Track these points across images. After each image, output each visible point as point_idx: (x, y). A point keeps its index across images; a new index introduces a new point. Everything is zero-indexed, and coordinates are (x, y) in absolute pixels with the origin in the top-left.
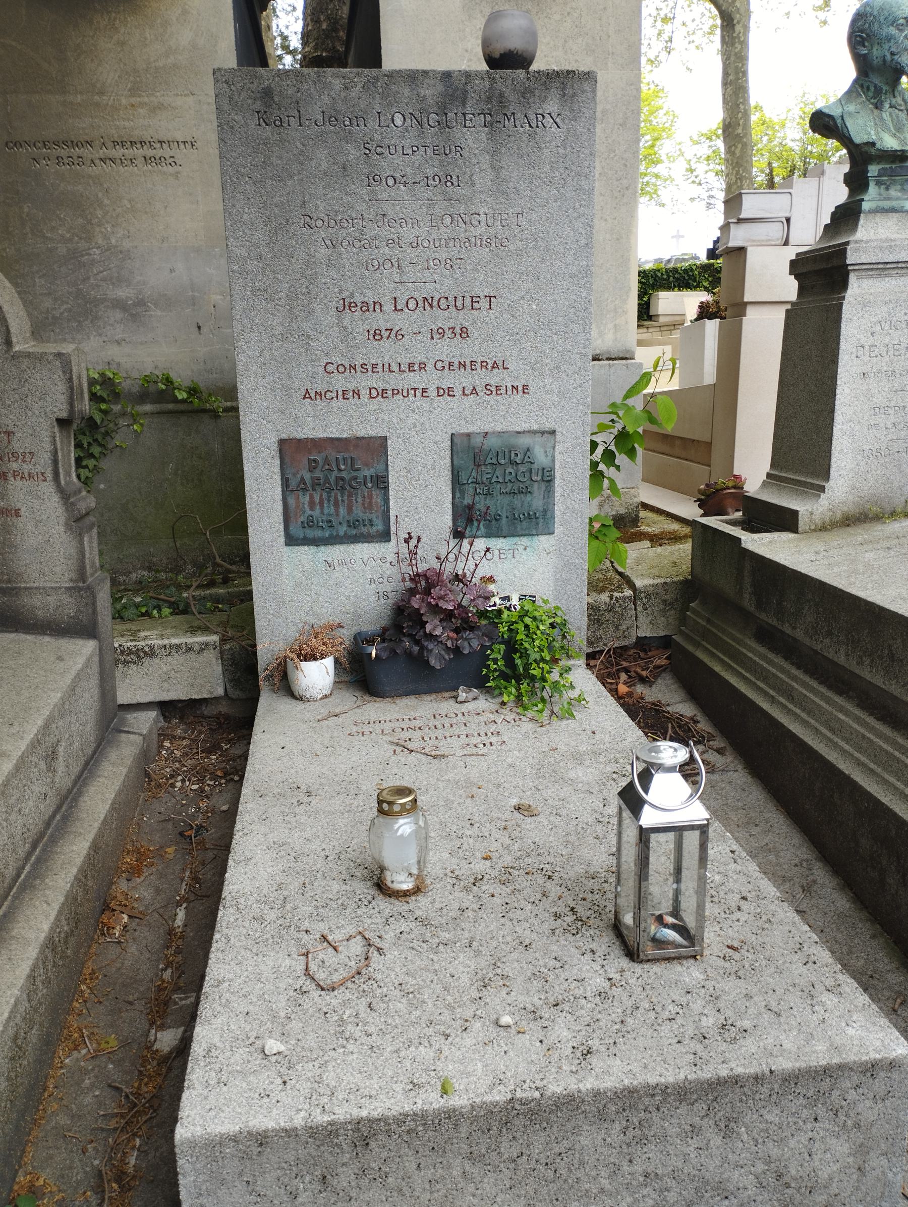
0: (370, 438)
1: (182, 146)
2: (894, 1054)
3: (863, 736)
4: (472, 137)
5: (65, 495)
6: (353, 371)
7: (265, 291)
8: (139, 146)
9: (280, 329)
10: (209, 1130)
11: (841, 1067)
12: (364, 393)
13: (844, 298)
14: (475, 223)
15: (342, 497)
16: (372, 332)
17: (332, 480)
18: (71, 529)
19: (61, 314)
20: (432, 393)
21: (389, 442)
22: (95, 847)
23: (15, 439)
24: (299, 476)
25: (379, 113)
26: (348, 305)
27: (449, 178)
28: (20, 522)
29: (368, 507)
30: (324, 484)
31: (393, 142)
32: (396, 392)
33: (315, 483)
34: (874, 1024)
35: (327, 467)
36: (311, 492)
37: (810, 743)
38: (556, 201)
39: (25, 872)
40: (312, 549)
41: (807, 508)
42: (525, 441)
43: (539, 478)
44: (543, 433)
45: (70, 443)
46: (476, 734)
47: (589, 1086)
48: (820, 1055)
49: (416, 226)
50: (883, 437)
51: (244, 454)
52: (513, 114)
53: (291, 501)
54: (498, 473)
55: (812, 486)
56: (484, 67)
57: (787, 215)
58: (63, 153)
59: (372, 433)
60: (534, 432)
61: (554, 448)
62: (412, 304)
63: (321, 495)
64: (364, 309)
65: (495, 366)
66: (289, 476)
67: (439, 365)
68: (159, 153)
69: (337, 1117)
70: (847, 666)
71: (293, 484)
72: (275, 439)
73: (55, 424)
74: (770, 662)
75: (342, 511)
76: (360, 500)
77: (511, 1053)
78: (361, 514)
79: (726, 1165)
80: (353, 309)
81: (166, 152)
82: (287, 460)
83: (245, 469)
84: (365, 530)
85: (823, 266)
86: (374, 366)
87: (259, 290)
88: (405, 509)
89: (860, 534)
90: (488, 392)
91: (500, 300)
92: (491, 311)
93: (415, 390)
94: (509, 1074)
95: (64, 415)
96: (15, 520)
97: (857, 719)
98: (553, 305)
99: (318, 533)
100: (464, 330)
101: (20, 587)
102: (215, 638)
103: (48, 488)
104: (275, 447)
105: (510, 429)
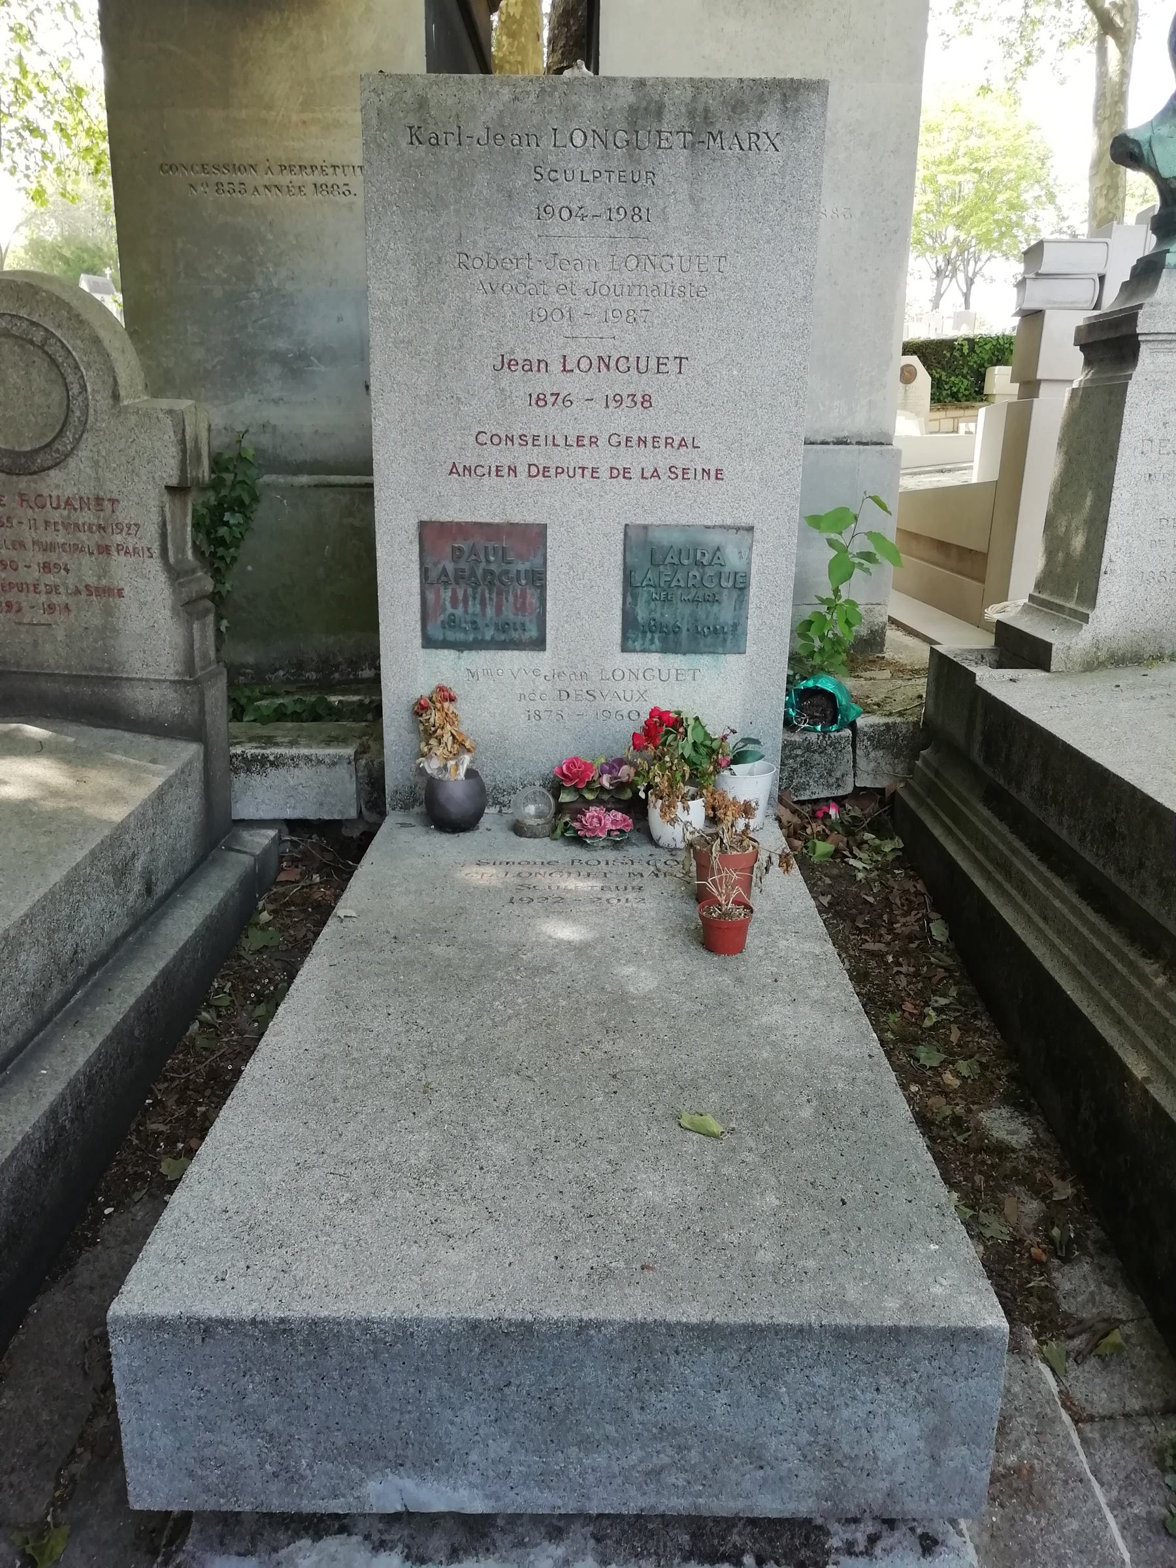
0: (527, 525)
2: (982, 1324)
3: (1076, 930)
4: (672, 163)
5: (175, 574)
6: (509, 443)
7: (410, 342)
8: (309, 170)
9: (426, 388)
10: (146, 1311)
11: (912, 1330)
12: (522, 470)
13: (1130, 377)
14: (666, 267)
15: (490, 594)
16: (534, 397)
17: (479, 572)
18: (178, 615)
19: (215, 367)
20: (604, 473)
21: (549, 531)
22: (166, 975)
23: (120, 508)
24: (440, 566)
25: (555, 130)
26: (508, 363)
27: (637, 210)
28: (122, 603)
30: (470, 578)
31: (570, 166)
32: (560, 470)
33: (459, 577)
34: (970, 1284)
35: (474, 557)
36: (455, 586)
37: (1019, 932)
38: (768, 242)
39: (76, 997)
41: (1066, 643)
42: (715, 538)
43: (730, 584)
44: (738, 529)
45: (185, 515)
46: (613, 888)
47: (593, 1316)
48: (889, 1311)
49: (593, 269)
50: (1170, 557)
51: (378, 537)
52: (720, 132)
53: (431, 596)
54: (679, 576)
55: (1074, 613)
57: (1102, 271)
58: (224, 178)
59: (530, 519)
60: (726, 528)
61: (751, 549)
62: (584, 364)
63: (465, 591)
64: (526, 368)
65: (683, 443)
66: (430, 566)
67: (614, 440)
68: (330, 179)
69: (291, 1313)
70: (1068, 841)
71: (434, 574)
73: (164, 491)
74: (993, 830)
75: (490, 611)
76: (511, 598)
77: (516, 1267)
78: (511, 616)
79: (761, 1429)
80: (513, 368)
81: (340, 179)
83: (378, 554)
84: (515, 635)
85: (1112, 335)
86: (535, 438)
87: (402, 342)
88: (565, 613)
89: (1127, 676)
90: (673, 476)
91: (692, 362)
92: (681, 376)
93: (583, 469)
94: (504, 1290)
95: (174, 482)
96: (117, 600)
97: (1073, 909)
98: (758, 371)
99: (460, 636)
100: (647, 398)
102: (349, 751)
103: (154, 566)
104: (413, 533)
105: (697, 522)
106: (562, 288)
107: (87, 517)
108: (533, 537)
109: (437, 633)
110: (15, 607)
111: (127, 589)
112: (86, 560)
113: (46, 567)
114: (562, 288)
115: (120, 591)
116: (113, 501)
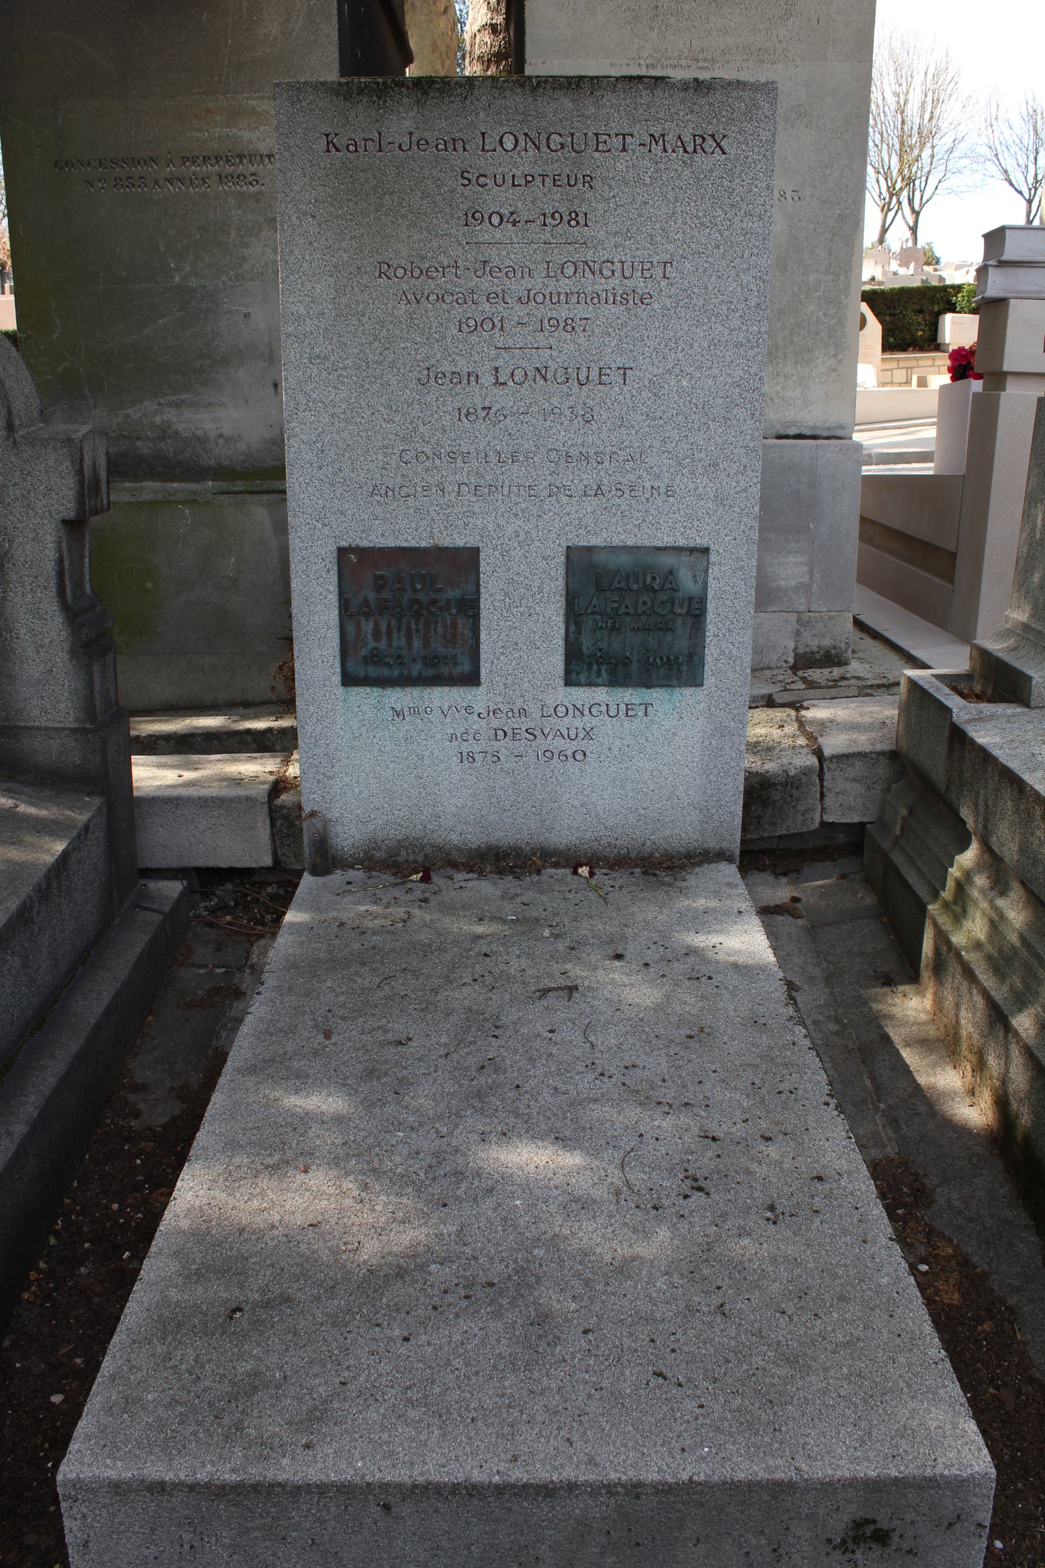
40: (376, 692)
59: (460, 543)
72: (333, 548)
75: (417, 644)
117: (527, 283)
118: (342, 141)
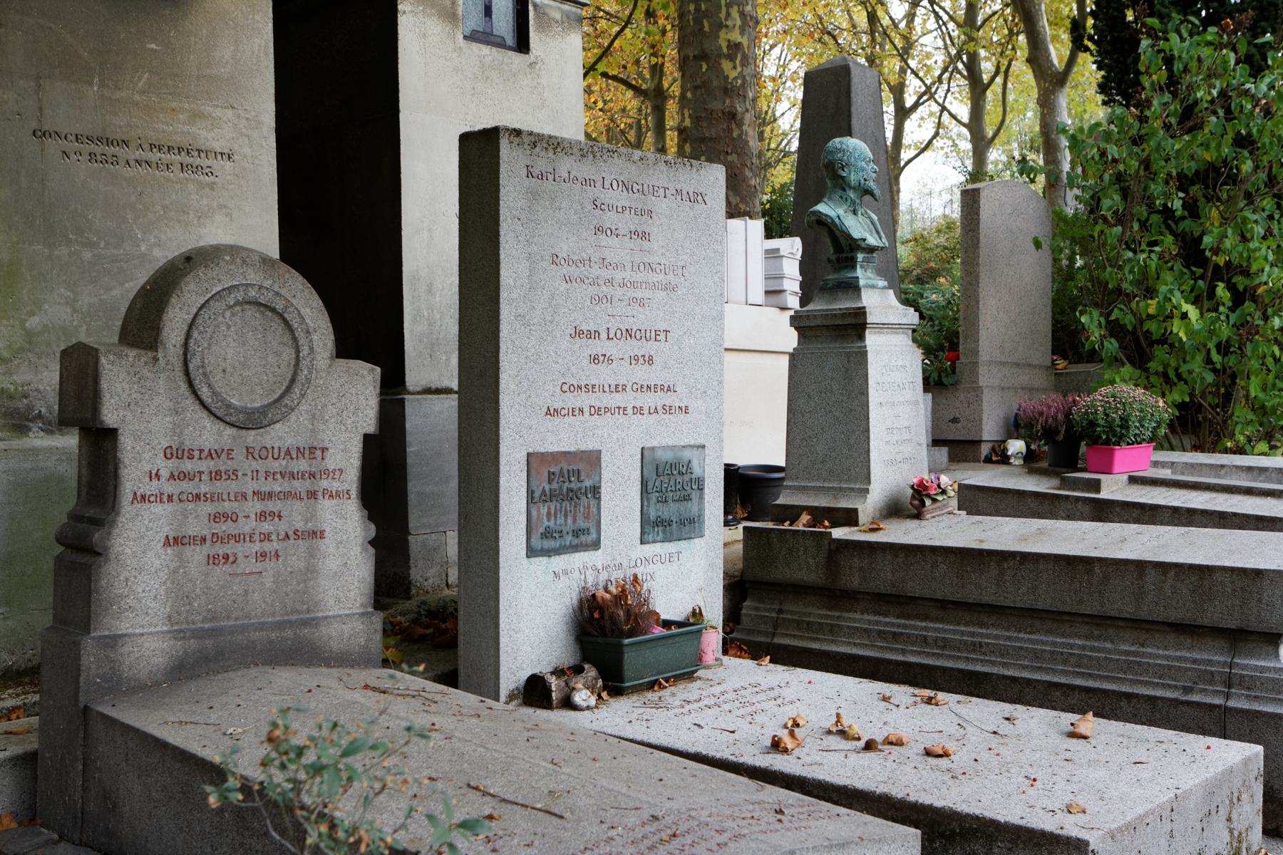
1: (219, 157)
20: (630, 411)
26: (578, 333)
29: (587, 517)
40: (544, 560)
42: (687, 454)
53: (534, 513)
56: (582, 138)
59: (590, 448)
60: (692, 447)
62: (619, 333)
71: (537, 495)
72: (525, 454)
75: (570, 521)
82: (533, 473)
86: (593, 386)
96: (320, 542)
101: (317, 618)
106: (610, 282)
107: (302, 465)
108: (593, 459)
109: (537, 543)
110: (231, 559)
111: (328, 530)
112: (298, 505)
113: (262, 516)
114: (610, 282)
115: (322, 532)
116: (324, 450)
117: (622, 275)
118: (536, 172)
